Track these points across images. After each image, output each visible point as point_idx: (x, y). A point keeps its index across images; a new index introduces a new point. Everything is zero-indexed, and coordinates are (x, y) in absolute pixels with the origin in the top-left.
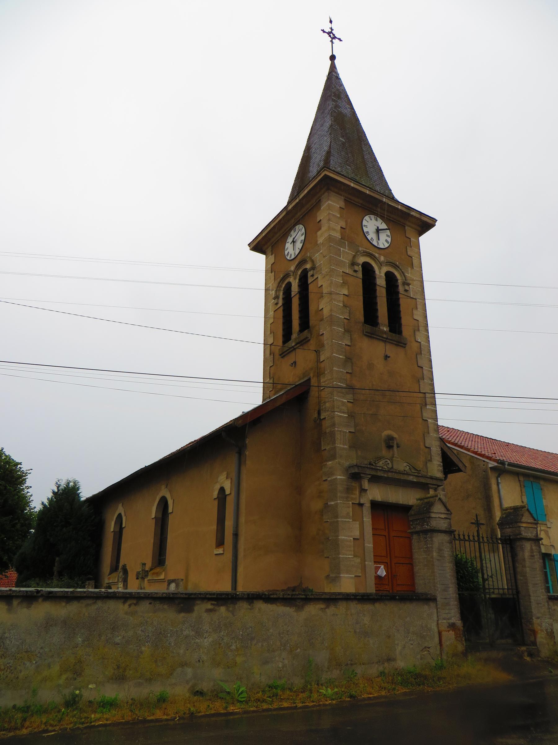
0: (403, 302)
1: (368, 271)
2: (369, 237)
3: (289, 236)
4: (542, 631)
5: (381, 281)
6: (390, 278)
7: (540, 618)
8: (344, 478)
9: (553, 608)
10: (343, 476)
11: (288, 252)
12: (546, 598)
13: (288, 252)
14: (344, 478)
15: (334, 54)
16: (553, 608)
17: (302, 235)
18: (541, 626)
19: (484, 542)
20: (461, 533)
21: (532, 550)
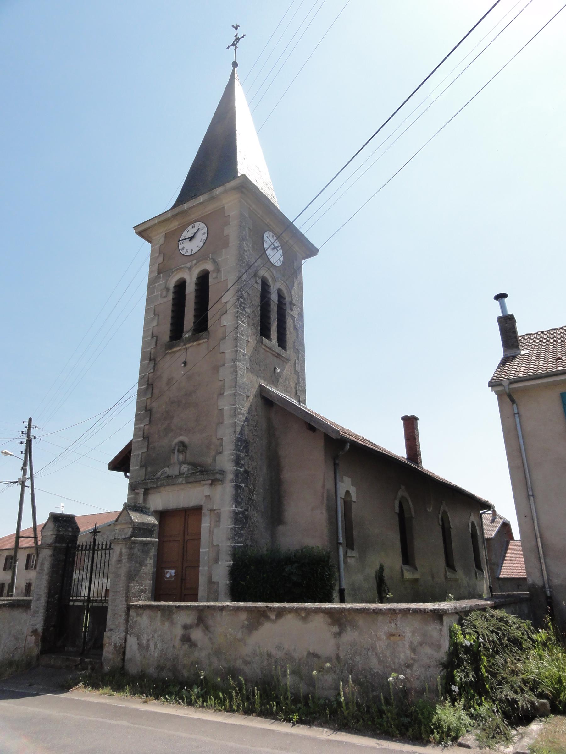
0: (289, 322)
1: (265, 286)
2: (205, 237)
3: (185, 231)
4: (110, 644)
5: (274, 297)
6: (281, 297)
7: (112, 630)
8: (132, 496)
9: (135, 619)
10: (132, 495)
11: (184, 247)
12: (125, 608)
13: (184, 247)
14: (132, 496)
15: (236, 61)
16: (135, 619)
17: (204, 234)
18: (110, 639)
19: (98, 550)
20: (100, 543)
21: (121, 554)
